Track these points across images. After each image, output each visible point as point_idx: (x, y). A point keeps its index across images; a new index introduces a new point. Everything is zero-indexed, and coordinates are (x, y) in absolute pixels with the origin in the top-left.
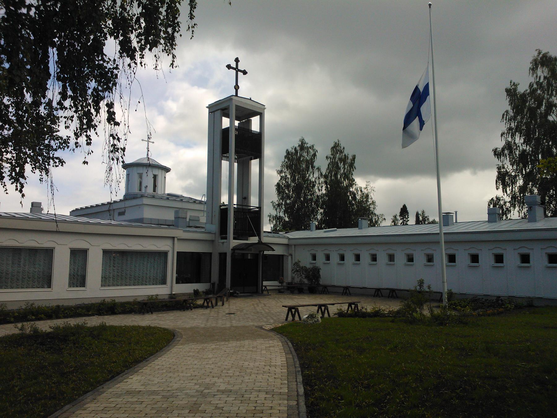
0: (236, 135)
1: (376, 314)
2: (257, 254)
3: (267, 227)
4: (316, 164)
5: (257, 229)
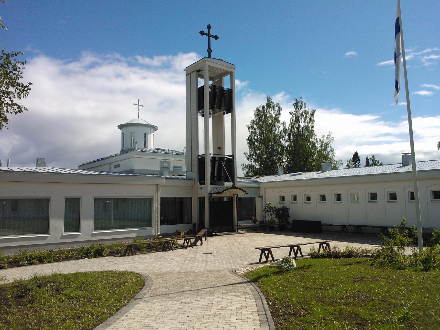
0: (209, 92)
1: (349, 255)
2: (232, 197)
3: (240, 172)
4: (281, 119)
5: (231, 176)
